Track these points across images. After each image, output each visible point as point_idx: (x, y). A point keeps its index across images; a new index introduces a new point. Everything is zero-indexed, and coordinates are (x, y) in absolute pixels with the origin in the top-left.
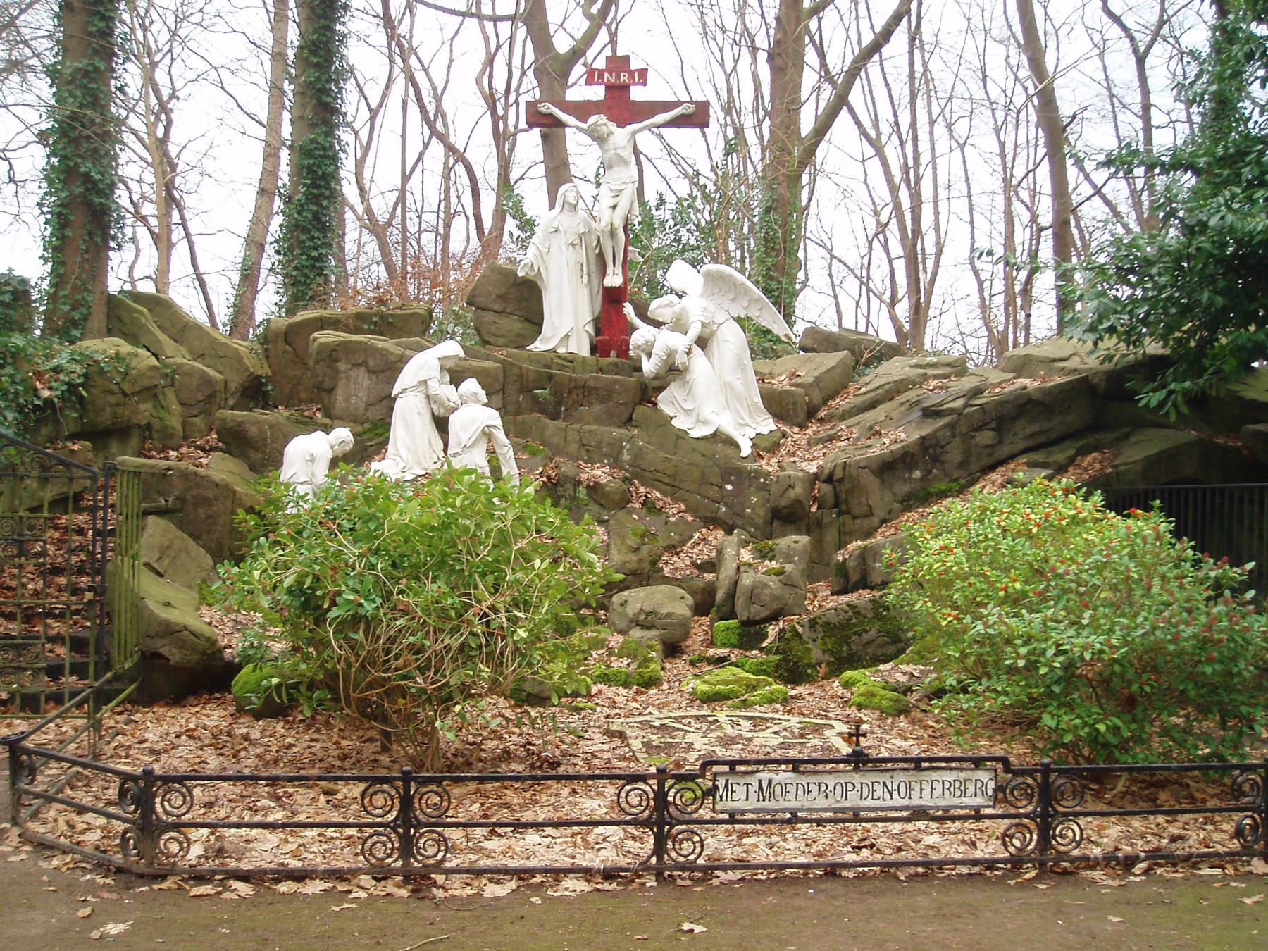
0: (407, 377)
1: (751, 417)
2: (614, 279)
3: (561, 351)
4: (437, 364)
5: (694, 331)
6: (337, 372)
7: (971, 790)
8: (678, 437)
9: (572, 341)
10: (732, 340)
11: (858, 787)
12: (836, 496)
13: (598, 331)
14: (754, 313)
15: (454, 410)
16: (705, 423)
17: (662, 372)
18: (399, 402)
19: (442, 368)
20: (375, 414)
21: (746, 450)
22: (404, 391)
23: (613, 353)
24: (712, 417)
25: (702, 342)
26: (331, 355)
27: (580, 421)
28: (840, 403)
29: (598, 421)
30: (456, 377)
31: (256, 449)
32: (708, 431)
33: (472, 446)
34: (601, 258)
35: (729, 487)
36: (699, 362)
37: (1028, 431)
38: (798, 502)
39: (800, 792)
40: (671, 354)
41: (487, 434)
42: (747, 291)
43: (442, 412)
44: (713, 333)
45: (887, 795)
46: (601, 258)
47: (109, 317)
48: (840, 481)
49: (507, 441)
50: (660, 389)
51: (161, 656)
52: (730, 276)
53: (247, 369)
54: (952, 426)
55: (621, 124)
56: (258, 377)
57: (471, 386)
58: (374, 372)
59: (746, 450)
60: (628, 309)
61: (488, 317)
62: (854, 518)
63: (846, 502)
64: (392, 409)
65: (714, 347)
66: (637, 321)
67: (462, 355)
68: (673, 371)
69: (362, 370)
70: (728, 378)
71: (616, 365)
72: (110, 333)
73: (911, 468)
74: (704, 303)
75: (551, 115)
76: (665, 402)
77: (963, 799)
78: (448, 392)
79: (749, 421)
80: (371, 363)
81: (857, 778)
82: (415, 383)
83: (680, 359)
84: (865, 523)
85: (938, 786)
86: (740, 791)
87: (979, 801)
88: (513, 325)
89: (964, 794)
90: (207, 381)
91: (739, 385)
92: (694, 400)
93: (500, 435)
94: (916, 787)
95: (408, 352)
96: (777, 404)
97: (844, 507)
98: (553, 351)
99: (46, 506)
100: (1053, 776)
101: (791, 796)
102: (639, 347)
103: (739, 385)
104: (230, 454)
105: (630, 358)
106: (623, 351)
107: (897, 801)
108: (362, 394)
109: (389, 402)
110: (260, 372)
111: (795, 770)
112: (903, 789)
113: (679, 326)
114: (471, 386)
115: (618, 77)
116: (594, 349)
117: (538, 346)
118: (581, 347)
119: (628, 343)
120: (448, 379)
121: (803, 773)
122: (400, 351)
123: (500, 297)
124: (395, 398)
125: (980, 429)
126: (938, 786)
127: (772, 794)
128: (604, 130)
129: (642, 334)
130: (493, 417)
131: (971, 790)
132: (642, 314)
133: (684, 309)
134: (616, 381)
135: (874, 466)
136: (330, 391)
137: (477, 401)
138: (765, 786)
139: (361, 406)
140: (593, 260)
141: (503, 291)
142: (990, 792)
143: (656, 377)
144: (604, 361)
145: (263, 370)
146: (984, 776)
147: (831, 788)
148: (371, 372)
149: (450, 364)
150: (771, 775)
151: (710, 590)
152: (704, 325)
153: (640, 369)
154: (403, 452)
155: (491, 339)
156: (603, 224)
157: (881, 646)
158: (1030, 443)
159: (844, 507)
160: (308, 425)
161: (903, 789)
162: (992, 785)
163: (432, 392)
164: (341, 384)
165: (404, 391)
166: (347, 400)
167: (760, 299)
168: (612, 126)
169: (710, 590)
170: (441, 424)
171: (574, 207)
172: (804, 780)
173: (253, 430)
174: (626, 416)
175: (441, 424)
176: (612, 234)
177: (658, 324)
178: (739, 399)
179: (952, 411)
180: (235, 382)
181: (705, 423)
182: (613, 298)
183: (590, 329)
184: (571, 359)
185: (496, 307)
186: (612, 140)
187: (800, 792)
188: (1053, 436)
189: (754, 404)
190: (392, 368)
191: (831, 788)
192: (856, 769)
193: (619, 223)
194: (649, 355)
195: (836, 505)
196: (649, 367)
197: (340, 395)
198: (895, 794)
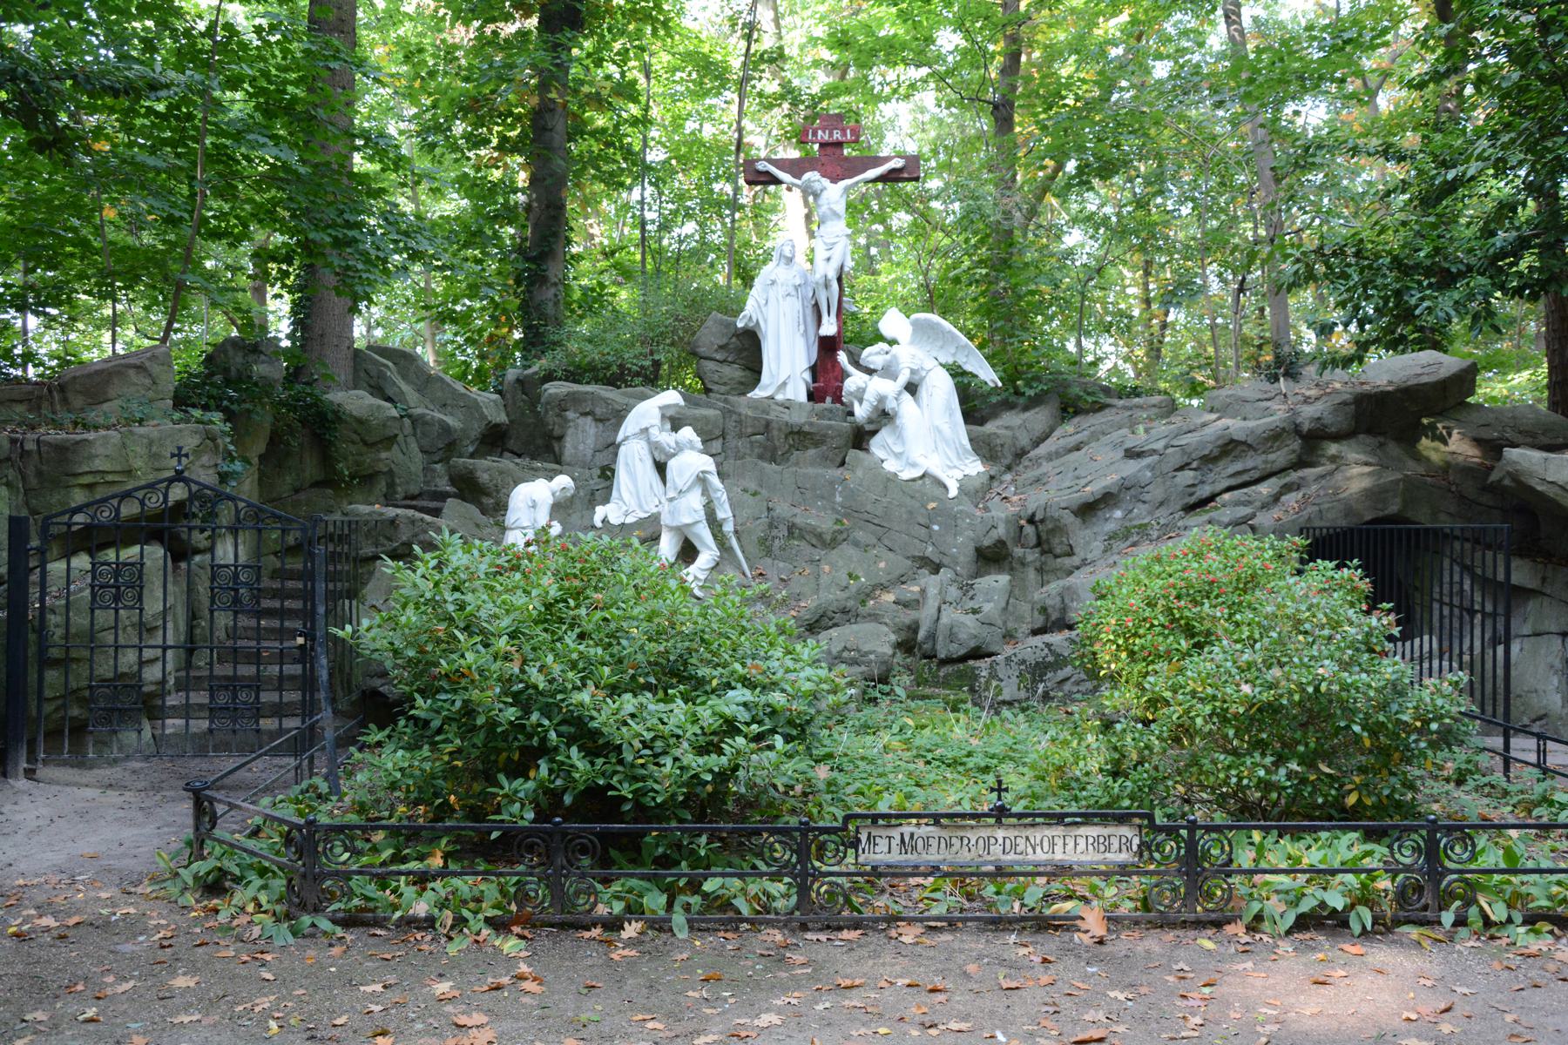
0: (630, 425)
1: (959, 458)
2: (829, 328)
3: (779, 397)
4: (657, 414)
5: (903, 378)
6: (566, 420)
7: (1115, 846)
8: (889, 480)
9: (789, 388)
10: (941, 388)
11: (1000, 841)
12: (1039, 536)
13: (815, 379)
14: (961, 360)
15: (674, 455)
16: (914, 465)
17: (874, 416)
18: (622, 449)
19: (663, 417)
20: (602, 459)
21: (953, 492)
22: (626, 438)
23: (829, 399)
24: (920, 460)
25: (912, 388)
26: (562, 405)
27: (797, 464)
28: (1042, 450)
29: (812, 464)
30: (676, 425)
31: (488, 495)
32: (917, 473)
33: (689, 490)
34: (816, 306)
35: (936, 527)
36: (907, 408)
37: (1231, 470)
38: (1001, 543)
39: (943, 845)
40: (882, 399)
41: (701, 480)
42: (953, 336)
43: (661, 458)
44: (923, 379)
45: (1030, 850)
46: (816, 306)
47: (356, 370)
48: (1042, 521)
49: (721, 486)
50: (874, 433)
51: (382, 695)
52: (938, 324)
53: (483, 417)
54: (1152, 468)
55: (834, 180)
56: (497, 425)
57: (687, 433)
58: (601, 420)
59: (953, 492)
60: (842, 357)
61: (710, 365)
62: (1056, 557)
63: (1048, 541)
64: (616, 455)
65: (923, 392)
66: (850, 369)
67: (682, 403)
68: (884, 416)
69: (589, 418)
70: (937, 423)
71: (831, 411)
72: (355, 388)
73: (1116, 506)
74: (913, 350)
75: (767, 173)
76: (877, 446)
77: (1107, 855)
78: (667, 438)
79: (956, 462)
80: (598, 411)
81: (1000, 834)
82: (637, 430)
83: (890, 405)
84: (1067, 562)
85: (1082, 842)
86: (882, 845)
87: (1124, 857)
88: (734, 372)
89: (1108, 849)
90: (446, 429)
91: (946, 428)
92: (903, 443)
93: (715, 480)
94: (1059, 842)
95: (631, 401)
96: (984, 448)
97: (1046, 547)
98: (771, 398)
99: (1453, 313)
100: (1199, 833)
101: (933, 849)
102: (851, 394)
103: (946, 428)
104: (464, 499)
105: (842, 403)
106: (838, 398)
107: (1041, 856)
108: (590, 441)
109: (613, 447)
110: (498, 420)
111: (937, 823)
112: (1046, 844)
113: (889, 372)
114: (687, 433)
115: (831, 135)
116: (811, 396)
117: (758, 393)
118: (798, 392)
119: (840, 389)
120: (668, 426)
121: (946, 827)
122: (626, 400)
123: (721, 347)
124: (619, 446)
125: (1181, 468)
126: (1082, 842)
127: (914, 848)
128: (817, 186)
129: (855, 380)
130: (707, 463)
131: (1115, 846)
132: (856, 363)
133: (895, 357)
134: (830, 427)
135: (1075, 507)
136: (560, 438)
137: (693, 448)
138: (907, 839)
139: (589, 452)
140: (809, 311)
141: (724, 341)
142: (1135, 848)
143: (870, 421)
144: (820, 406)
145: (502, 418)
146: (1126, 831)
147: (973, 842)
148: (598, 420)
149: (670, 413)
150: (911, 829)
151: (914, 628)
152: (913, 372)
153: (851, 414)
154: (625, 495)
155: (715, 387)
156: (818, 276)
157: (1078, 683)
158: (1233, 482)
159: (1046, 547)
160: (533, 475)
161: (1046, 844)
162: (1136, 841)
163: (653, 439)
164: (570, 432)
165: (626, 438)
166: (576, 448)
167: (966, 346)
168: (826, 182)
169: (914, 628)
170: (661, 468)
171: (790, 260)
172: (945, 834)
173: (484, 478)
174: (839, 460)
175: (661, 468)
176: (827, 286)
177: (870, 372)
178: (946, 442)
179: (1154, 451)
180: (476, 429)
181: (914, 465)
182: (828, 346)
183: (807, 376)
184: (787, 405)
185: (718, 357)
186: (825, 195)
187: (943, 845)
188: (1256, 475)
189: (962, 446)
190: (619, 416)
191: (973, 842)
192: (999, 822)
193: (832, 275)
194: (861, 401)
195: (1039, 544)
196: (861, 412)
197: (569, 443)
198: (1038, 849)
